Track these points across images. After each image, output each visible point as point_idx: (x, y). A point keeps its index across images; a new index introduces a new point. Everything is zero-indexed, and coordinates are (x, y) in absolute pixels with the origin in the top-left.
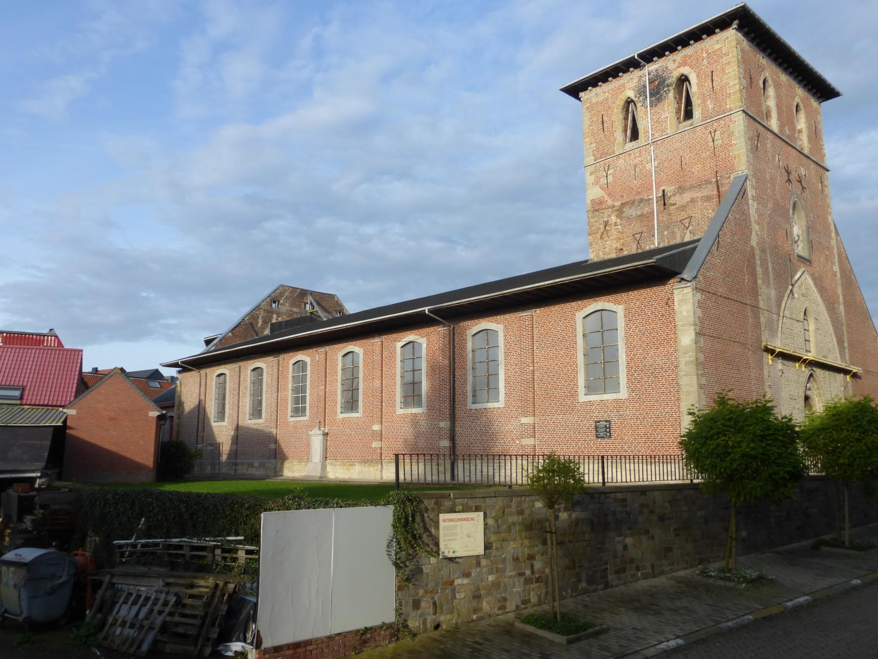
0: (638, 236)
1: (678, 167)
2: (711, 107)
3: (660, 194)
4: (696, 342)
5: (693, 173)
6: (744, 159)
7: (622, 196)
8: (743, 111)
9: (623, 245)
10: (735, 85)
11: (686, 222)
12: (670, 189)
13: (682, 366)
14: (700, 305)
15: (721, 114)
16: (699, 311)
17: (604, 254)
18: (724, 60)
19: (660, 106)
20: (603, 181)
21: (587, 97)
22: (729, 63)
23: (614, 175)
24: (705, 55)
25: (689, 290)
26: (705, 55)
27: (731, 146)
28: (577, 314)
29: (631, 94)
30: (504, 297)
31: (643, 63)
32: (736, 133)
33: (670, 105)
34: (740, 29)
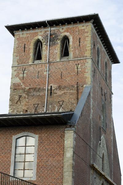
0: (36, 105)
1: (60, 76)
2: (77, 53)
3: (50, 88)
4: (73, 156)
5: (66, 81)
6: (90, 80)
7: (30, 85)
8: (92, 58)
9: (28, 108)
10: (89, 47)
11: (61, 103)
12: (54, 86)
13: (65, 167)
14: (75, 139)
15: (81, 58)
16: (75, 142)
17: (17, 111)
18: (86, 35)
19: (53, 47)
20: (21, 75)
21: (18, 33)
22: (88, 36)
23: (27, 74)
24: (77, 30)
25: (72, 131)
26: (77, 30)
27: (85, 72)
28: (13, 136)
29: (40, 38)
30: (19, 116)
31: (48, 26)
32: (88, 67)
33: (57, 49)
34: (93, 23)
